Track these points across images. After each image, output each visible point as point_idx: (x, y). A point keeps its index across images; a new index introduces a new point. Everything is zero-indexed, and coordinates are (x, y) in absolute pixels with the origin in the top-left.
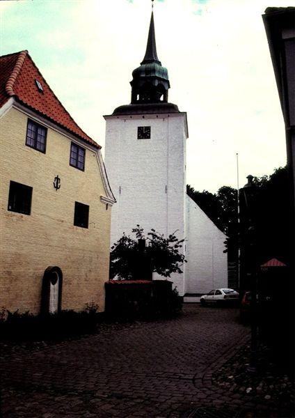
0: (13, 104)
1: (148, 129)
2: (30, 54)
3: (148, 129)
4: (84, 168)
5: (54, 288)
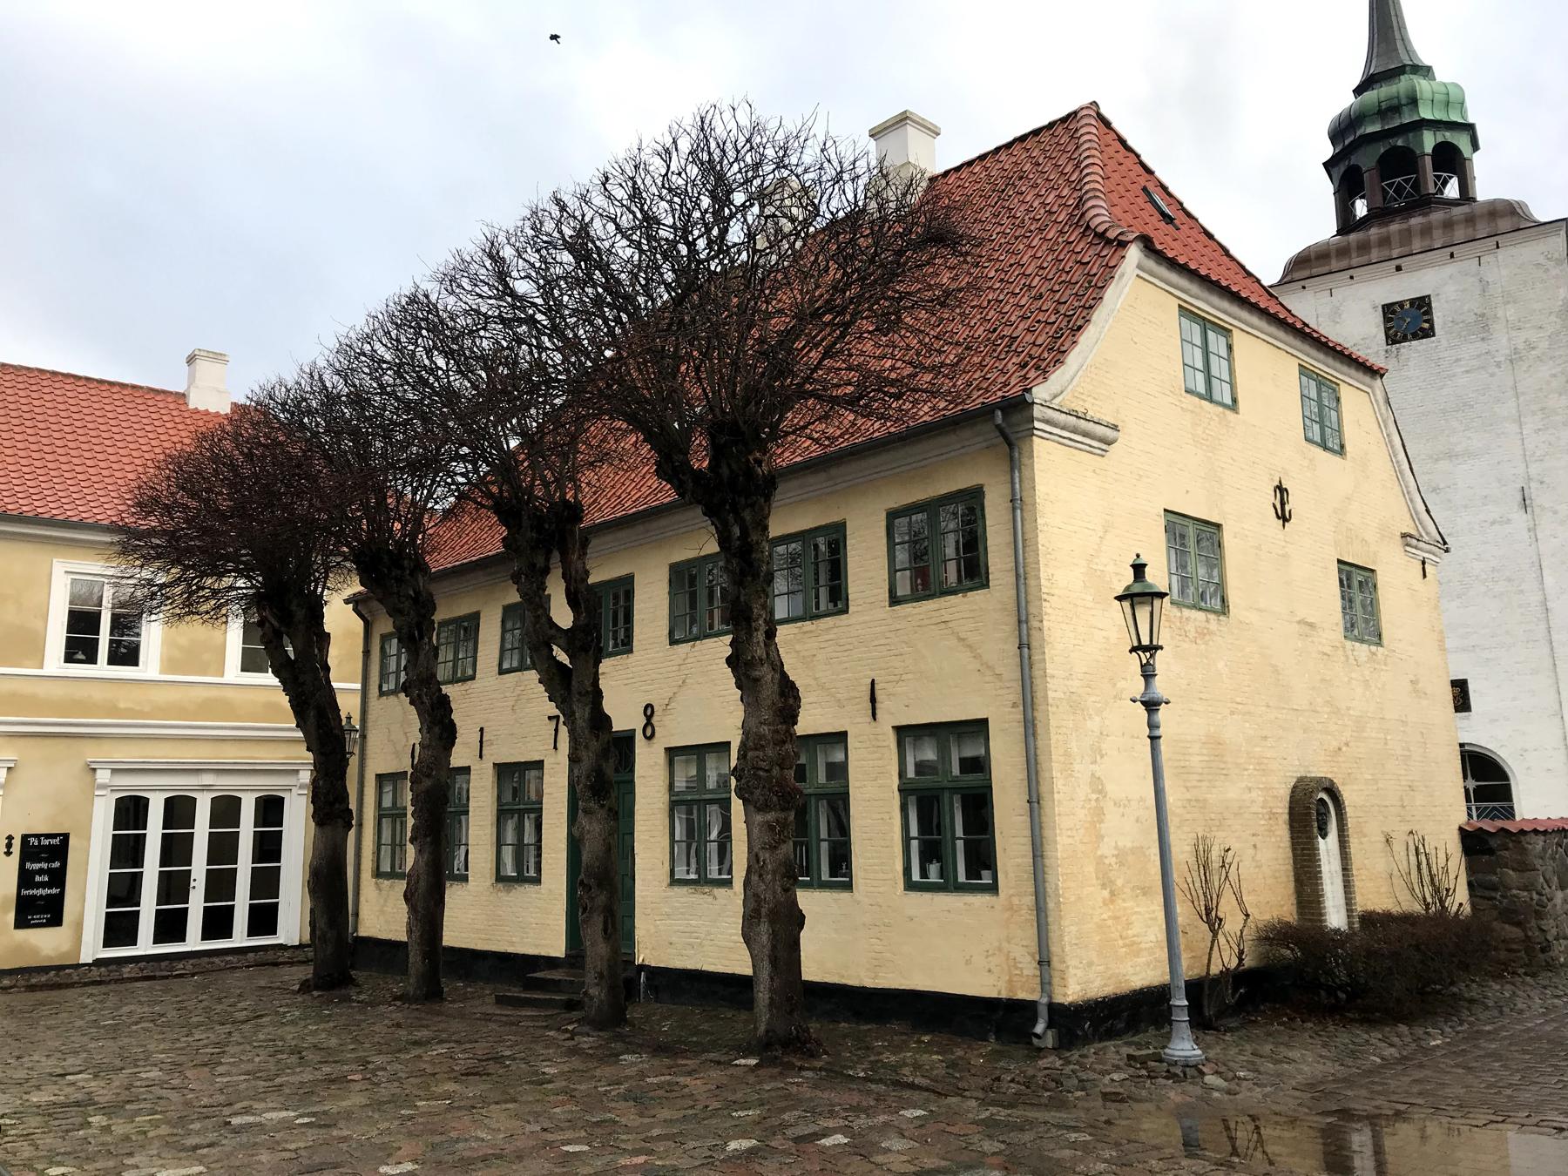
0: (1139, 267)
1: (1422, 305)
2: (1103, 111)
3: (1422, 305)
4: (1342, 447)
5: (1327, 847)
